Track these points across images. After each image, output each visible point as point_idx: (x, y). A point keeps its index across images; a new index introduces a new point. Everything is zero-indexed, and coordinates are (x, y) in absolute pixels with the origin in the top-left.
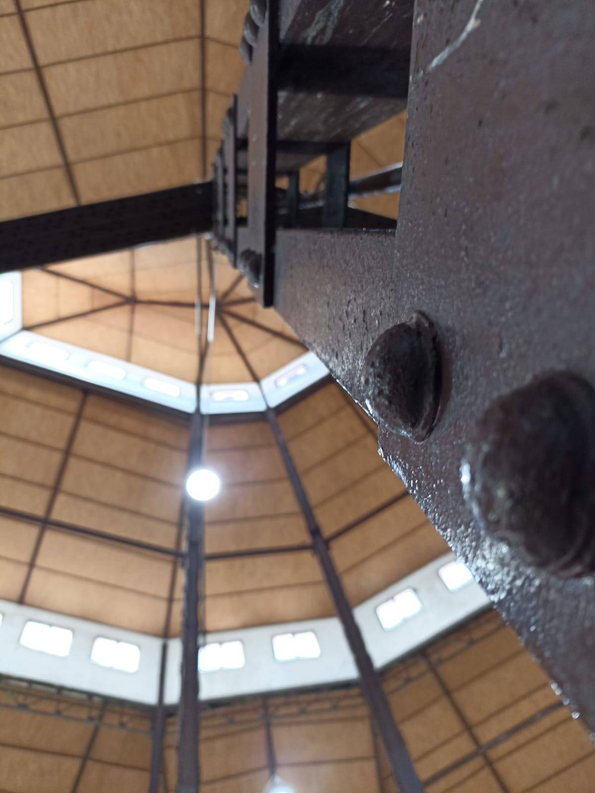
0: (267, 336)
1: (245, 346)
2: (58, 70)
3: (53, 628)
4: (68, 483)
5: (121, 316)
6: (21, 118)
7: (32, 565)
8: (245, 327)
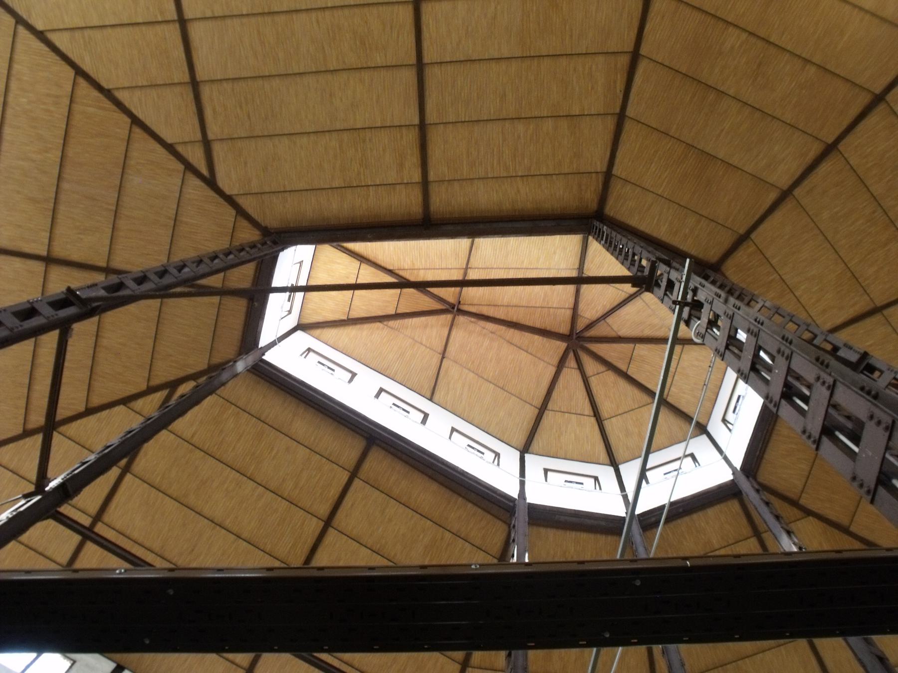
6: (379, 60)
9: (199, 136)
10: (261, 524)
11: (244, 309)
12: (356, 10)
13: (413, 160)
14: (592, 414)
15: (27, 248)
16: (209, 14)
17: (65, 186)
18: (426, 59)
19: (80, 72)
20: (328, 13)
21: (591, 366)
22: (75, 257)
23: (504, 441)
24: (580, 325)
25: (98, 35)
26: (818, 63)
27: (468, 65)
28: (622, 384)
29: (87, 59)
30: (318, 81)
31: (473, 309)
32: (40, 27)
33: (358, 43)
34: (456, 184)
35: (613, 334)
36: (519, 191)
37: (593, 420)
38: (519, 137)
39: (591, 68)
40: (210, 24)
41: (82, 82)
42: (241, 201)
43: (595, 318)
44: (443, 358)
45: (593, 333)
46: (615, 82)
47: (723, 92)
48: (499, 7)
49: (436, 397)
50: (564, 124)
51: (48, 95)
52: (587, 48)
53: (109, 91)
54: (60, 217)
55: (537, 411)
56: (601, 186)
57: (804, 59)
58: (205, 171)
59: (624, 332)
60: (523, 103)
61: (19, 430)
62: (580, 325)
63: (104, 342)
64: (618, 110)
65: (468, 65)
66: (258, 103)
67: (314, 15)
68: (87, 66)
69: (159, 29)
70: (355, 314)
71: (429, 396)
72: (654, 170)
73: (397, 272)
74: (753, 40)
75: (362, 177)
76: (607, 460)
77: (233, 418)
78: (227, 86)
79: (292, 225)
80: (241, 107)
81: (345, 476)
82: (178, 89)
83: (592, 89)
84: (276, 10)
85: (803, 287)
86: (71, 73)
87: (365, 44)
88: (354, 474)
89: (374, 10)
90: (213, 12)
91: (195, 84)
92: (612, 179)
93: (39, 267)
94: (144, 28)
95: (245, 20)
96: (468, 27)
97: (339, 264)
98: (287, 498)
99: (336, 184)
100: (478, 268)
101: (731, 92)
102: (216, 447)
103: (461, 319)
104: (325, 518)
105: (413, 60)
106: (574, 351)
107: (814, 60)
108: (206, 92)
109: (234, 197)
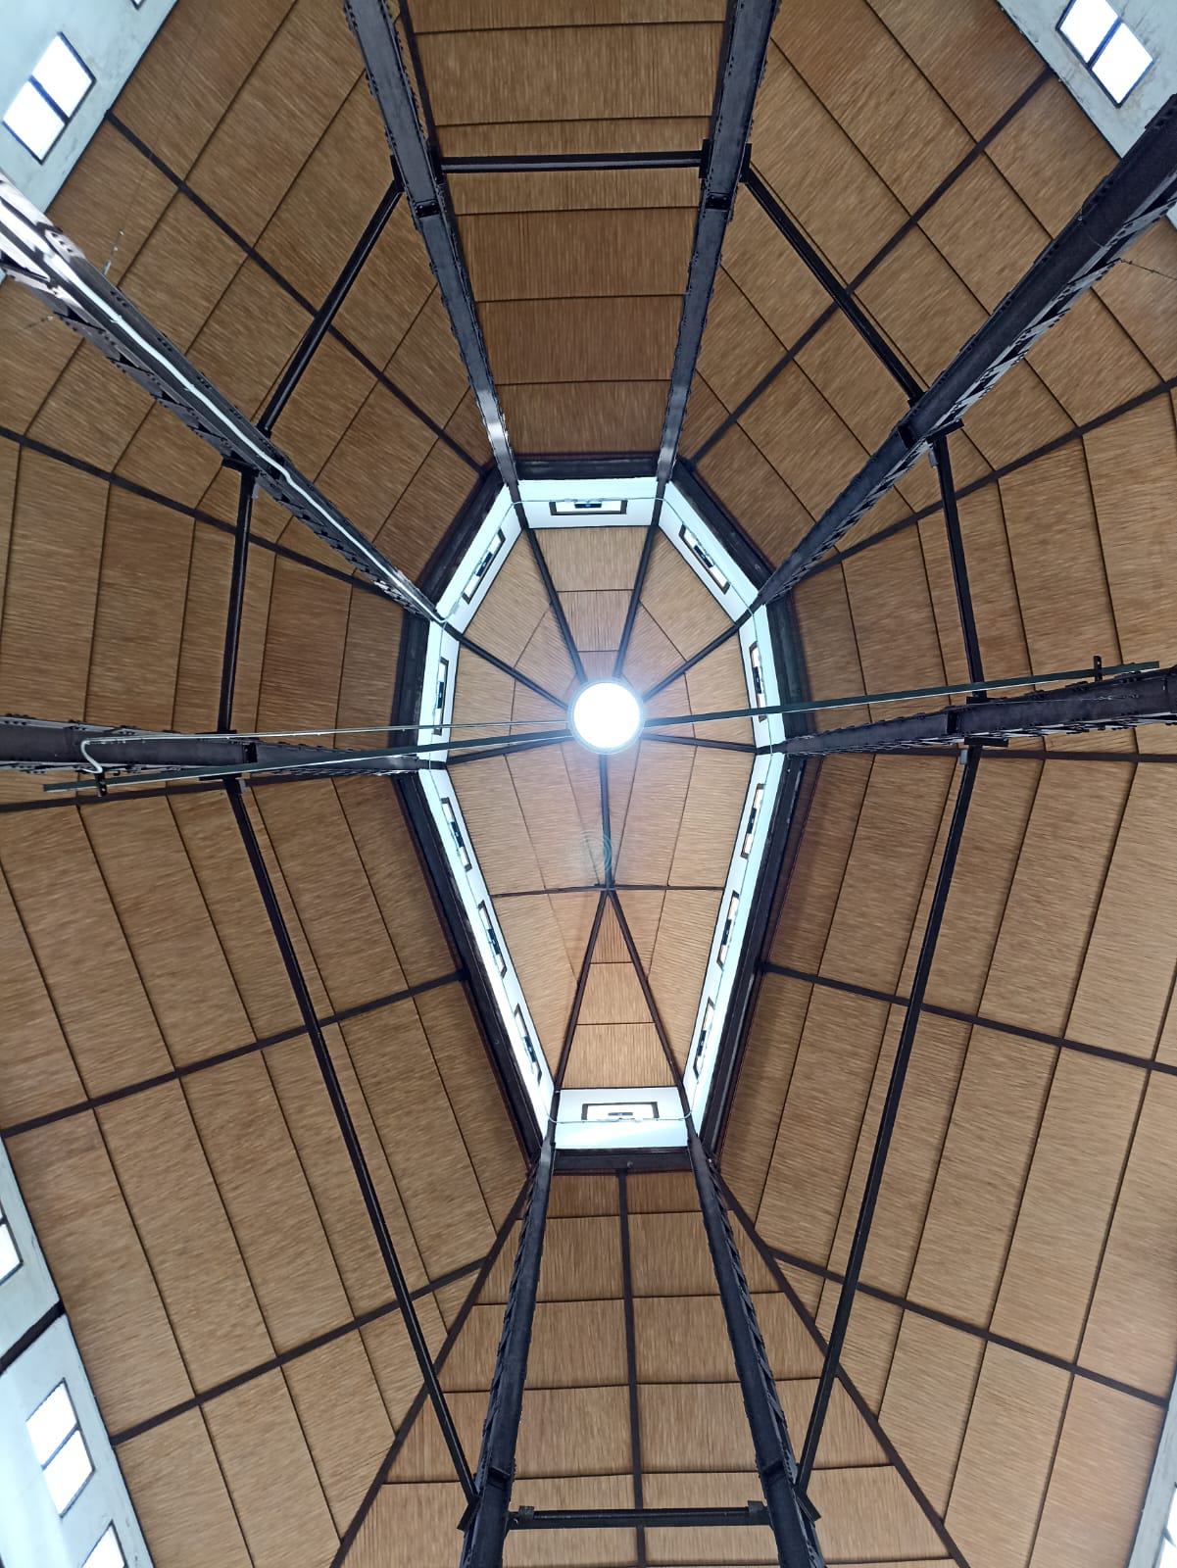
6: (267, 1098)
11: (641, 1178)
12: (209, 1145)
13: (385, 1016)
14: (682, 677)
16: (262, 1328)
18: (251, 1040)
19: (382, 1479)
22: (625, 1434)
25: (326, 1468)
26: (98, 570)
30: (315, 1165)
32: (335, 1544)
34: (402, 954)
36: (390, 875)
37: (689, 674)
38: (318, 897)
39: (204, 839)
40: (274, 1323)
41: (395, 1472)
42: (500, 1220)
47: (178, 672)
48: (158, 973)
51: (420, 1515)
52: (178, 852)
53: (397, 1433)
54: (576, 1466)
55: (699, 749)
57: (99, 589)
58: (474, 1276)
61: (891, 1471)
67: (229, 1196)
69: (297, 1388)
70: (646, 1015)
71: (720, 893)
73: (578, 975)
74: (98, 658)
76: (734, 638)
78: (351, 1279)
81: (821, 990)
82: (372, 1343)
84: (234, 1245)
85: (390, 485)
86: (386, 1490)
87: (252, 1121)
88: (815, 979)
89: (203, 1123)
90: (258, 1324)
95: (258, 1281)
96: (195, 1002)
98: (874, 1062)
99: (444, 1102)
101: (174, 662)
104: (886, 1003)
107: (97, 576)
109: (498, 1229)
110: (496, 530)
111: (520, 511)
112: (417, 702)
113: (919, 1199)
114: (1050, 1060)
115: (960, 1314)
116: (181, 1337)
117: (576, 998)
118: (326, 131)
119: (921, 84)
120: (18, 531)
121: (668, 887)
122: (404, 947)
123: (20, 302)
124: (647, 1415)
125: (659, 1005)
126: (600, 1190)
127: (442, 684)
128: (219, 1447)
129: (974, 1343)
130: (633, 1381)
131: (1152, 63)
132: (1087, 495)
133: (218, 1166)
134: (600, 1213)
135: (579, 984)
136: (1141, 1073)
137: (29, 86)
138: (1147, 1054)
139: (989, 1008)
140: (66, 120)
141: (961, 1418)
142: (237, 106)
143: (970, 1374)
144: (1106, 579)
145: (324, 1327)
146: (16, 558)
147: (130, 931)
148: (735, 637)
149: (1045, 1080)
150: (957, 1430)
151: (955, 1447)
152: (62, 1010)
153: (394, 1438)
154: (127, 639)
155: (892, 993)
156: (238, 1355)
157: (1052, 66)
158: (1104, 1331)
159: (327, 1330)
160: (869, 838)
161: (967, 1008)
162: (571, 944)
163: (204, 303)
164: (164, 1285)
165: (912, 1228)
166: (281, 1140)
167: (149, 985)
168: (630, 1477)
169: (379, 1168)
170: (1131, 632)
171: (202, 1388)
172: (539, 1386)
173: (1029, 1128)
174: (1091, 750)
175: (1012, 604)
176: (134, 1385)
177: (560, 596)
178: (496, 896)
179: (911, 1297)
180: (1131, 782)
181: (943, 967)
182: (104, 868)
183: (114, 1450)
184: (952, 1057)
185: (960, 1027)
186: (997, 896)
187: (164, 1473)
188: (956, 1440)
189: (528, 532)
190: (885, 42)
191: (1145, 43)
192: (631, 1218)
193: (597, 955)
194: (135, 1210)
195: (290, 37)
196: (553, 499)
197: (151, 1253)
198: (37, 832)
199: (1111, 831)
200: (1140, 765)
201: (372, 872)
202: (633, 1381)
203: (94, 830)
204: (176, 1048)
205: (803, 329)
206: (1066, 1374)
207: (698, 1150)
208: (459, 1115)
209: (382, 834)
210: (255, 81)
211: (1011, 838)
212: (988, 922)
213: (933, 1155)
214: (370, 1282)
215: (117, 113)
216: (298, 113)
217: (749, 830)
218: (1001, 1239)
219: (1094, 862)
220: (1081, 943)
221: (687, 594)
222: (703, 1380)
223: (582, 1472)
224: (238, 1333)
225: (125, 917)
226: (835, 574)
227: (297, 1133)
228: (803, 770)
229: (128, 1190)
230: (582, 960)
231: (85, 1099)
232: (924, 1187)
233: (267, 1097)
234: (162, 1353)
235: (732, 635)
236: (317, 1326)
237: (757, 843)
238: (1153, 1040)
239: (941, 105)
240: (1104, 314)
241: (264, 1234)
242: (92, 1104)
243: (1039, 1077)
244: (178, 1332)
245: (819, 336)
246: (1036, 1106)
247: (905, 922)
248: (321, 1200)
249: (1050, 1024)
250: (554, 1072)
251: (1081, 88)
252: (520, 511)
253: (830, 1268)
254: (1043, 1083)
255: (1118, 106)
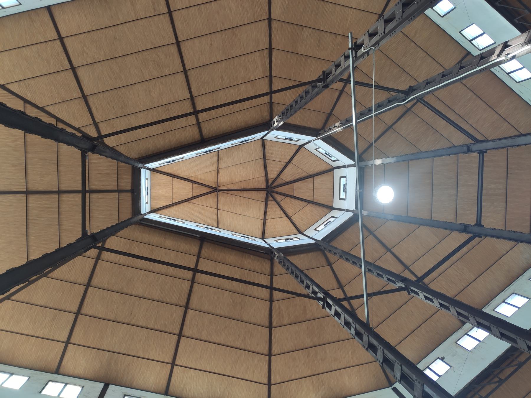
0: (304, 203)
1: (290, 212)
2: (189, 43)
3: (522, 70)
4: (194, 302)
5: (210, 200)
6: (167, 72)
7: (173, 364)
8: (288, 199)
9: (92, 122)
10: (162, 291)
14: (285, 216)
15: (15, 189)
16: (85, 63)
17: (29, 155)
18: (187, 68)
20: (140, 54)
21: (279, 198)
22: (41, 189)
23: (253, 236)
24: (270, 181)
25: (32, 82)
27: (205, 67)
28: (293, 200)
29: (29, 95)
31: (224, 188)
33: (156, 65)
35: (284, 182)
36: (237, 119)
37: (286, 218)
38: (232, 95)
39: (254, 59)
43: (275, 178)
44: (218, 209)
45: (276, 184)
46: (265, 62)
49: (220, 226)
50: (249, 84)
52: (251, 50)
53: (42, 108)
54: (29, 171)
55: (263, 221)
56: (269, 109)
59: (288, 180)
60: (231, 79)
62: (270, 181)
63: (63, 227)
64: (269, 75)
65: (205, 67)
66: (117, 101)
67: (134, 56)
68: (29, 98)
69: (62, 74)
70: (175, 201)
72: (288, 96)
74: (314, 31)
75: (171, 126)
77: (137, 247)
78: (100, 95)
79: (144, 155)
80: (109, 104)
82: (77, 101)
83: (256, 67)
87: (159, 66)
89: (160, 49)
90: (87, 62)
91: (85, 97)
92: (273, 104)
93: (23, 197)
94: (55, 75)
95: (103, 63)
97: (163, 180)
100: (223, 168)
102: (132, 262)
103: (220, 193)
105: (182, 70)
106: (270, 194)
108: (91, 100)
109: (114, 147)
110: (339, 159)
111: (344, 167)
112: (291, 132)
113: (125, 290)
114: (174, 332)
115: (85, 304)
116: (85, 34)
117: (181, 177)
118: (460, 116)
119: (462, 288)
120: (355, 10)
121: (218, 209)
122: (213, 122)
123: (421, 20)
124: (48, 197)
125: (178, 206)
126: (126, 183)
127: (292, 139)
128: (43, 44)
129: (75, 309)
130: (60, 192)
131: (469, 351)
132: (348, 338)
133: (145, 53)
134: (119, 183)
135: (185, 178)
136: (170, 361)
137: (482, 32)
138: (177, 363)
139: (190, 312)
140: (470, 41)
141: (47, 305)
142: (469, 90)
143: (63, 308)
144: (324, 345)
145: (84, 85)
146: (347, 8)
147: (227, 32)
148: (298, 233)
149: (167, 331)
150: (42, 304)
151: (36, 303)
152: (202, 6)
153: (41, 107)
154: (319, 41)
155: (195, 281)
156: (76, 54)
157: (466, 324)
158: (81, 353)
159: (83, 86)
160: (244, 274)
161: (190, 306)
162: (199, 177)
163: (416, 76)
164: (104, 30)
165: (115, 288)
166: (152, 75)
167: (208, 36)
168: (25, 190)
169: (139, 108)
170: (308, 353)
171: (65, 40)
172: (58, 159)
173: (151, 326)
174: (272, 342)
175: (316, 317)
176: (68, 16)
177: (313, 178)
178: (218, 153)
179: (90, 288)
180: (262, 354)
181: (204, 297)
182: (247, 25)
183: (45, 7)
184: (174, 301)
185: (184, 303)
186: (227, 314)
187: (35, 24)
188: (39, 303)
189: (333, 169)
190: (473, 278)
191: (474, 348)
192: (117, 194)
193: (195, 185)
194: (131, 23)
195: (485, 107)
196: (348, 177)
197: (116, 27)
198: (261, 4)
199: (247, 349)
200: (268, 357)
201: (239, 113)
202: (60, 192)
203: (260, 23)
204: (186, 42)
205: (397, 254)
206: (65, 339)
207: (140, 217)
208: (155, 136)
209: (251, 117)
210: (475, 96)
211: (245, 318)
212: (218, 312)
213: (141, 295)
214: (99, 102)
215: (470, 56)
216: (465, 108)
217: (242, 236)
218: (112, 318)
219: (238, 344)
220: (212, 341)
221: (311, 218)
222: (60, 216)
223: (27, 173)
224: (84, 55)
225: (231, 30)
226: (325, 263)
227: (154, 81)
228: (265, 253)
229: (139, 21)
230: (194, 180)
231: (172, 10)
232: (130, 292)
233: (167, 72)
234: (79, 27)
235: (299, 232)
236: (84, 82)
237: (238, 237)
238: (181, 364)
239: (457, 294)
240: (399, 341)
241: (119, 66)
242: (170, 12)
243: (168, 329)
244: (86, 34)
245: (395, 259)
246: (159, 328)
247: (218, 285)
248: (129, 87)
249: (187, 331)
250: (157, 169)
251: (460, 332)
252: (344, 167)
253: (100, 261)
254: (166, 330)
255: (456, 342)
